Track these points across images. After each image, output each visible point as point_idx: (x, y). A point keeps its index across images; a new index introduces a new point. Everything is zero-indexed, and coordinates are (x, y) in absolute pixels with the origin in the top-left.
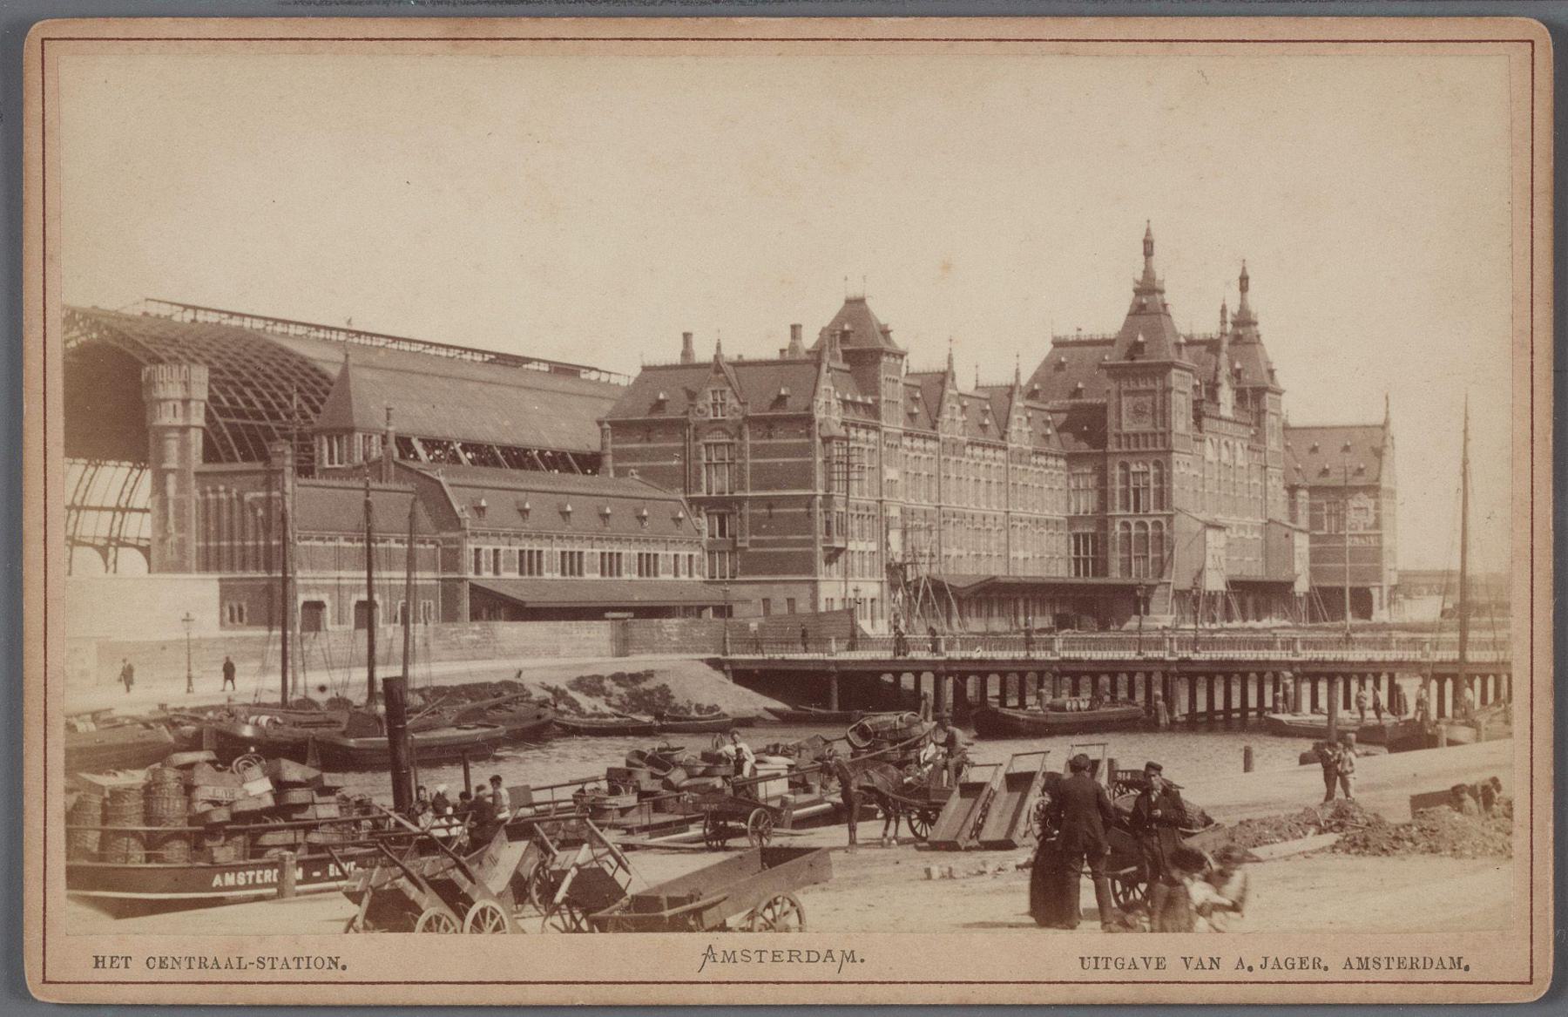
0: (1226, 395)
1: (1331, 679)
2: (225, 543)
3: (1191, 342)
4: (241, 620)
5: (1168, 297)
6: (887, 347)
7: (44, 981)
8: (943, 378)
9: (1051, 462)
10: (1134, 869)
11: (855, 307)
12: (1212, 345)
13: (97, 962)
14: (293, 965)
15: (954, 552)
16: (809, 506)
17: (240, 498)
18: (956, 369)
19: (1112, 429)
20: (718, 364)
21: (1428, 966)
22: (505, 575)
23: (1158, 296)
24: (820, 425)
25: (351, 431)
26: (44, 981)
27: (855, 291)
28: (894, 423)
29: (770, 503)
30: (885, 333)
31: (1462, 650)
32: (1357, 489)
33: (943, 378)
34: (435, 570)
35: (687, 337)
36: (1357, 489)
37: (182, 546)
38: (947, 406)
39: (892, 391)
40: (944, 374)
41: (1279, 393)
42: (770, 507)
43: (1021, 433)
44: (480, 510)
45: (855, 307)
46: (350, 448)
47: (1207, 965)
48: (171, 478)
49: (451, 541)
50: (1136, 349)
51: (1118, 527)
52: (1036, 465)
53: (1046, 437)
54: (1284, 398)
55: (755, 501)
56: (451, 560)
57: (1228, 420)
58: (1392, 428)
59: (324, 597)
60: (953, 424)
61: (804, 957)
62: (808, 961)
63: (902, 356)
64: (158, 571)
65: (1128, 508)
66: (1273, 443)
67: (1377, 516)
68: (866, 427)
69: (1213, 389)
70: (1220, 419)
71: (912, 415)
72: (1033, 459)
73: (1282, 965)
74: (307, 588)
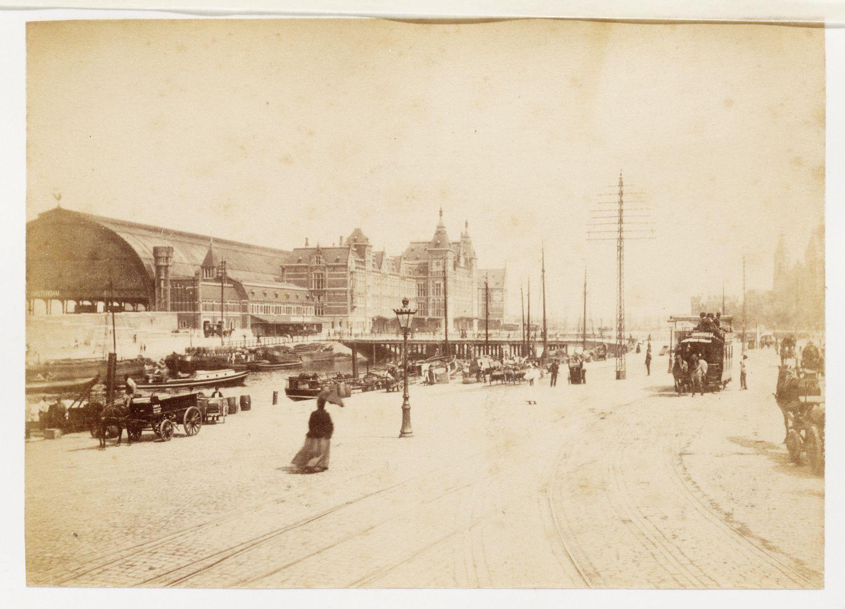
0: (462, 260)
1: (480, 346)
2: (184, 303)
4: (185, 326)
6: (475, 257)
8: (383, 254)
9: (412, 280)
11: (358, 232)
12: (458, 244)
16: (346, 293)
19: (430, 270)
22: (260, 313)
23: (444, 229)
24: (350, 268)
25: (213, 267)
27: (357, 226)
29: (334, 292)
31: (487, 338)
32: (496, 289)
33: (383, 254)
34: (240, 311)
36: (496, 289)
38: (383, 262)
39: (369, 257)
41: (371, 246)
44: (253, 293)
45: (358, 232)
50: (437, 245)
51: (431, 301)
53: (393, 269)
57: (463, 267)
60: (385, 269)
64: (159, 310)
65: (434, 295)
66: (475, 274)
69: (458, 258)
71: (373, 265)
74: (204, 317)
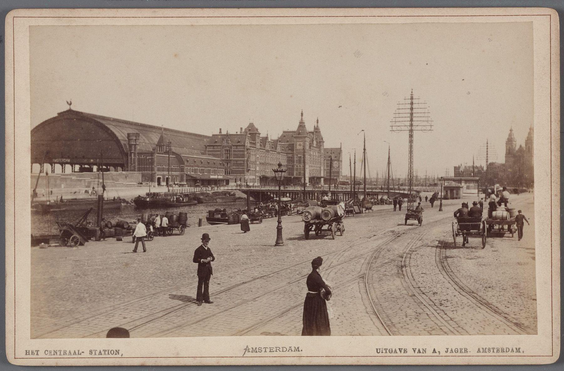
0: (315, 142)
3: (309, 133)
5: (305, 124)
7: (15, 358)
8: (267, 138)
11: (251, 125)
12: (312, 133)
14: (103, 353)
15: (267, 171)
17: (146, 158)
18: (268, 136)
20: (227, 135)
22: (192, 173)
26: (15, 358)
27: (251, 121)
28: (258, 146)
29: (237, 161)
30: (257, 130)
33: (267, 138)
34: (179, 172)
35: (220, 129)
37: (134, 166)
38: (267, 143)
39: (258, 140)
41: (324, 142)
42: (237, 161)
43: (279, 149)
45: (251, 125)
46: (163, 148)
48: (133, 154)
49: (183, 167)
52: (261, 151)
54: (324, 143)
55: (234, 161)
56: (182, 170)
57: (315, 147)
58: (342, 149)
59: (161, 177)
60: (268, 147)
61: (281, 350)
62: (283, 351)
67: (339, 165)
68: (253, 147)
69: (313, 141)
70: (314, 147)
72: (260, 150)
73: (454, 351)
74: (158, 175)
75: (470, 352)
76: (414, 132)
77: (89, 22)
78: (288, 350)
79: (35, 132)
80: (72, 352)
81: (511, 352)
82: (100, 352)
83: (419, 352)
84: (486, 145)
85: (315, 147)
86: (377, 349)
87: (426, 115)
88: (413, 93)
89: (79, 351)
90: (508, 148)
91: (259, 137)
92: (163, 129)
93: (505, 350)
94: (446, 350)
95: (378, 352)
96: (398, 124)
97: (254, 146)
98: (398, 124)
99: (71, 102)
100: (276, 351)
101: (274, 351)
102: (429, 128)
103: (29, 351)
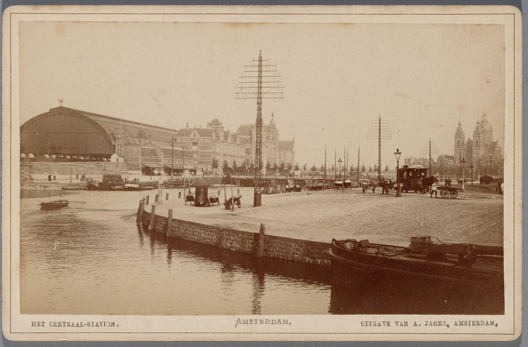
8: (229, 131)
10: (478, 255)
13: (33, 324)
21: (483, 324)
33: (229, 131)
40: (228, 131)
47: (404, 324)
54: (279, 136)
57: (271, 140)
60: (230, 139)
61: (271, 322)
63: (223, 128)
73: (433, 324)
75: (420, 325)
76: (263, 99)
77: (80, 18)
78: (277, 322)
79: (22, 128)
80: (75, 325)
81: (486, 325)
82: (97, 324)
83: (402, 325)
84: (378, 122)
85: (271, 140)
86: (362, 322)
87: (277, 79)
88: (261, 56)
89: (81, 323)
90: (457, 141)
91: (222, 130)
92: (142, 124)
93: (480, 323)
94: (426, 323)
95: (363, 325)
96: (244, 90)
97: (219, 139)
98: (244, 90)
99: (62, 100)
100: (266, 323)
101: (263, 323)
102: (279, 95)
103: (35, 322)
